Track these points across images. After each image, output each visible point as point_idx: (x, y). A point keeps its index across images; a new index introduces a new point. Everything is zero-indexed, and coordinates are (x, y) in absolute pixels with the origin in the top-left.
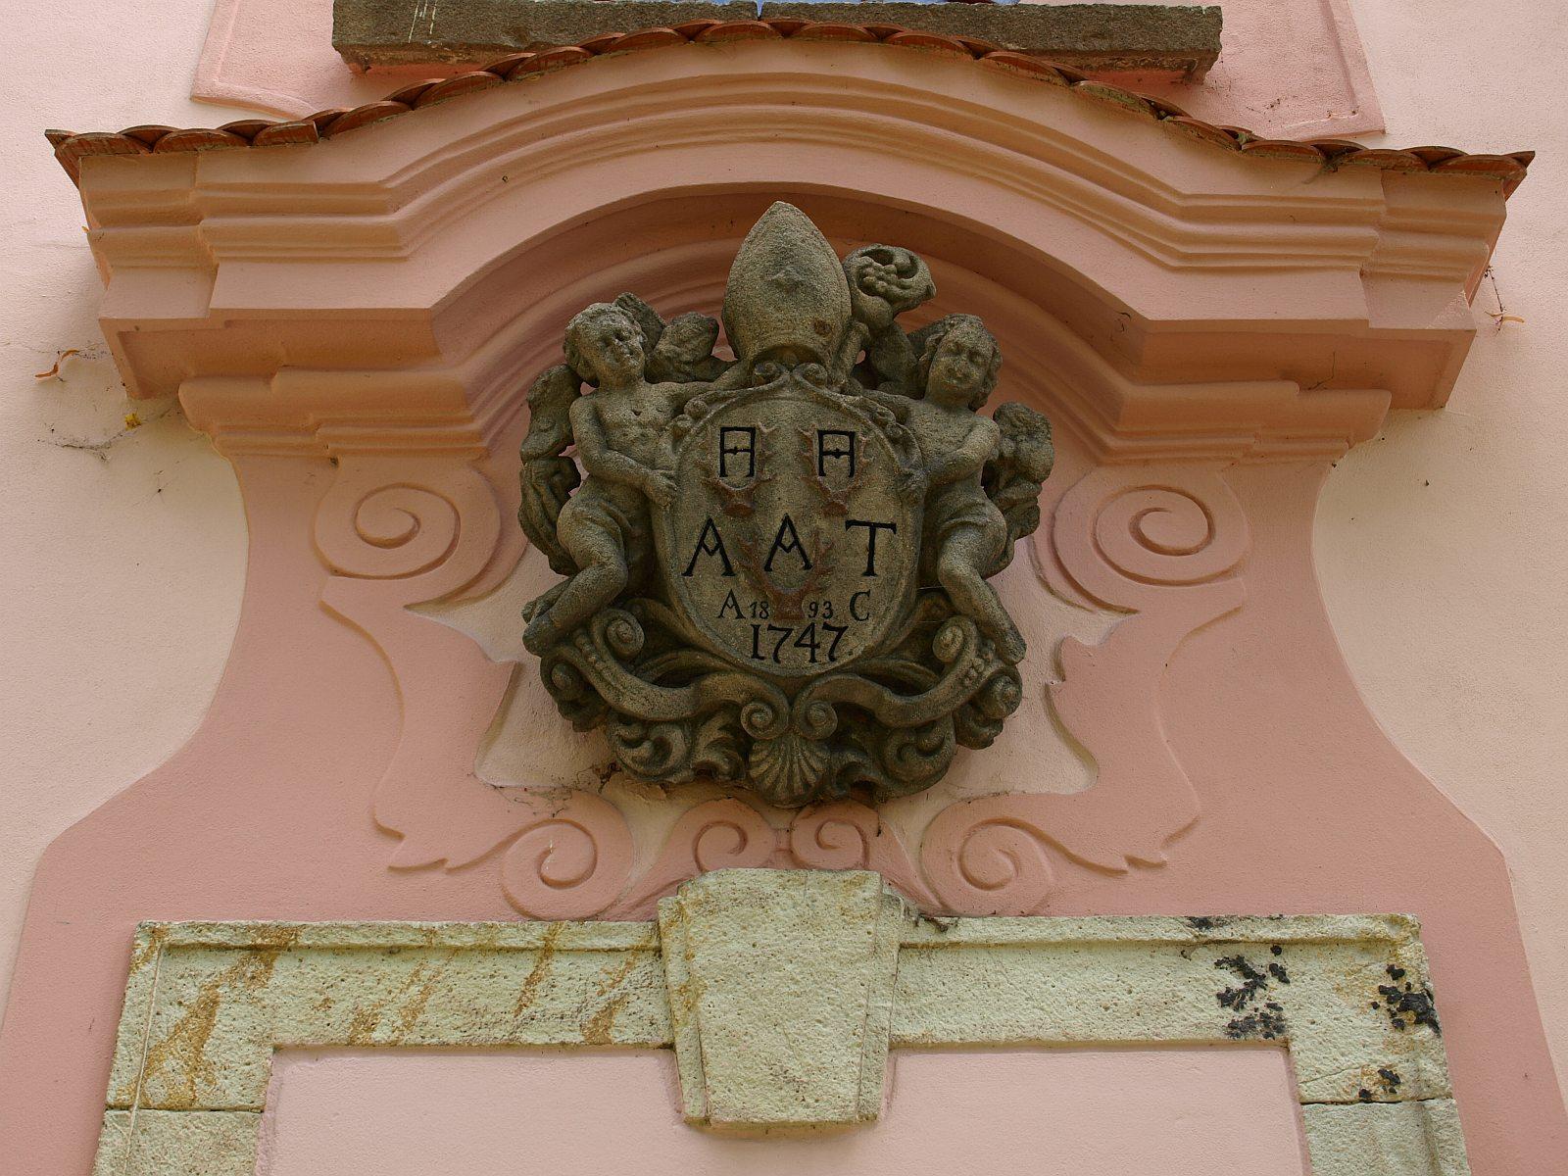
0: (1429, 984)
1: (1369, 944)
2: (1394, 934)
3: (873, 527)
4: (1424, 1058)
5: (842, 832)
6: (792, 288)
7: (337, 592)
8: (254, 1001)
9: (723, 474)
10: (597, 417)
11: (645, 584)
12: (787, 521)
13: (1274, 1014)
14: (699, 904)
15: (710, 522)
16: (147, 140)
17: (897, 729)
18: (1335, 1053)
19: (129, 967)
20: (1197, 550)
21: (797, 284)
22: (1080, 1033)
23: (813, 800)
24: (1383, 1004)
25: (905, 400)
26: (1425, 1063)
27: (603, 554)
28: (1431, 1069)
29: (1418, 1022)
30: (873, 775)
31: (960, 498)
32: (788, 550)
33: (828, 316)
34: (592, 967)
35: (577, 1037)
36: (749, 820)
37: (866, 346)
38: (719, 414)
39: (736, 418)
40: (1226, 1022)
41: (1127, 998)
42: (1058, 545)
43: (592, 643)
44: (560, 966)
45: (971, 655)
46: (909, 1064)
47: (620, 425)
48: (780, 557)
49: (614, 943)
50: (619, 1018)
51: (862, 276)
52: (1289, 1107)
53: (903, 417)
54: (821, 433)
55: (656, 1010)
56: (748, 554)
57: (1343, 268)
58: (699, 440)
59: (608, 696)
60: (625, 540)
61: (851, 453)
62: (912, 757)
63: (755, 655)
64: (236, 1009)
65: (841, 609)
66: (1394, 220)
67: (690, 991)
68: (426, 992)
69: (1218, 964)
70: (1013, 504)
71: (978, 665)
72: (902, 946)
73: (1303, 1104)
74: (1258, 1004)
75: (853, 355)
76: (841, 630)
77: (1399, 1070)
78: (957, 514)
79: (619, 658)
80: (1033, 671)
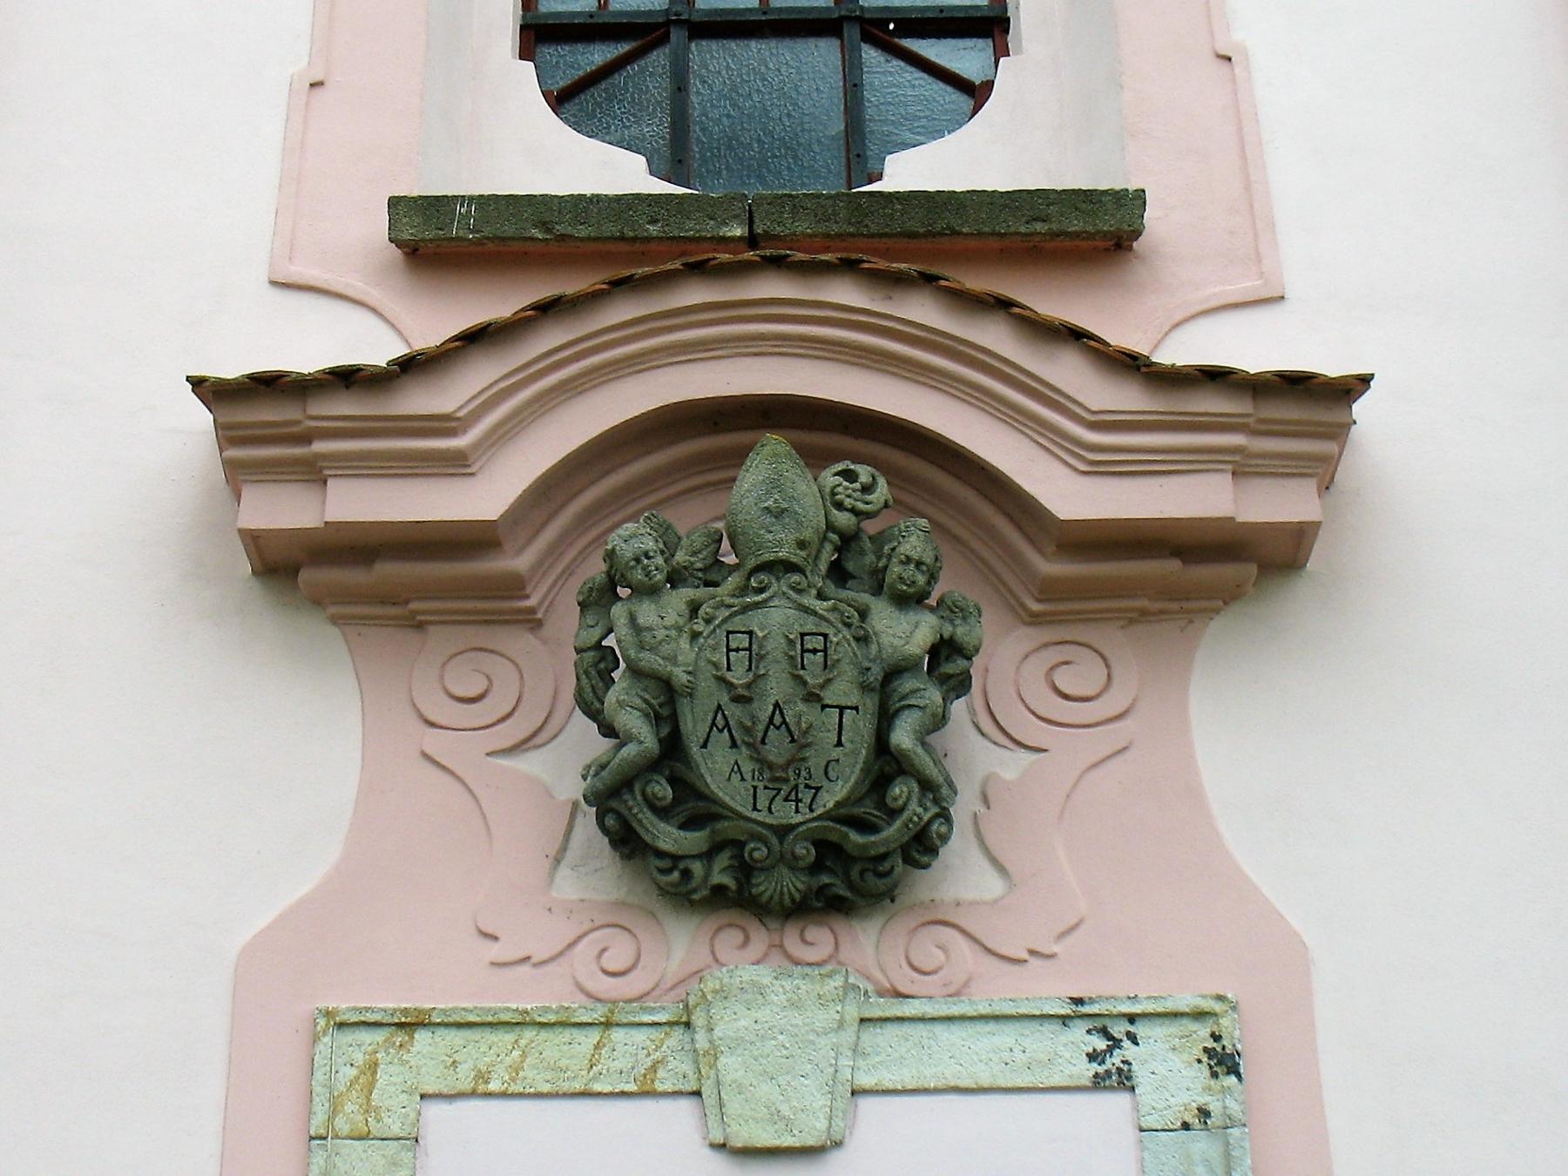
0: (1239, 1047)
1: (1200, 1015)
2: (1217, 1007)
3: (842, 709)
4: (1225, 1098)
5: (819, 939)
6: (779, 514)
7: (435, 742)
8: (403, 1063)
9: (729, 669)
10: (632, 619)
11: (673, 749)
12: (777, 705)
13: (1125, 1068)
14: (715, 992)
15: (719, 707)
16: (267, 385)
17: (860, 859)
18: (1167, 1095)
19: (315, 1039)
20: (1098, 696)
21: (784, 510)
22: (986, 1082)
23: (800, 910)
24: (1205, 1059)
25: (865, 598)
26: (1230, 1103)
27: (645, 739)
28: (1234, 1107)
29: (1228, 1073)
30: (842, 891)
31: (907, 684)
32: (778, 728)
33: (807, 534)
34: (640, 1036)
35: (632, 1087)
36: (754, 927)
37: (838, 549)
38: (725, 621)
39: (738, 623)
40: (1091, 1073)
41: (1022, 1056)
42: (990, 695)
43: (635, 799)
44: (618, 1035)
45: (914, 806)
46: (865, 1103)
47: (650, 629)
48: (772, 733)
49: (656, 1019)
50: (661, 1073)
51: (833, 494)
52: (1131, 1134)
53: (863, 614)
54: (803, 635)
55: (687, 1067)
56: (748, 731)
57: (1217, 471)
58: (710, 641)
59: (648, 838)
60: (656, 719)
61: (825, 651)
62: (869, 876)
63: (755, 809)
64: (391, 1069)
65: (818, 772)
66: (1263, 427)
67: (714, 1054)
68: (524, 1055)
69: (1089, 1032)
70: (950, 677)
71: (918, 812)
72: (862, 1020)
73: (1142, 1130)
74: (1115, 1060)
75: (828, 555)
76: (818, 789)
77: (1211, 1108)
78: (904, 698)
79: (654, 809)
80: (963, 809)
